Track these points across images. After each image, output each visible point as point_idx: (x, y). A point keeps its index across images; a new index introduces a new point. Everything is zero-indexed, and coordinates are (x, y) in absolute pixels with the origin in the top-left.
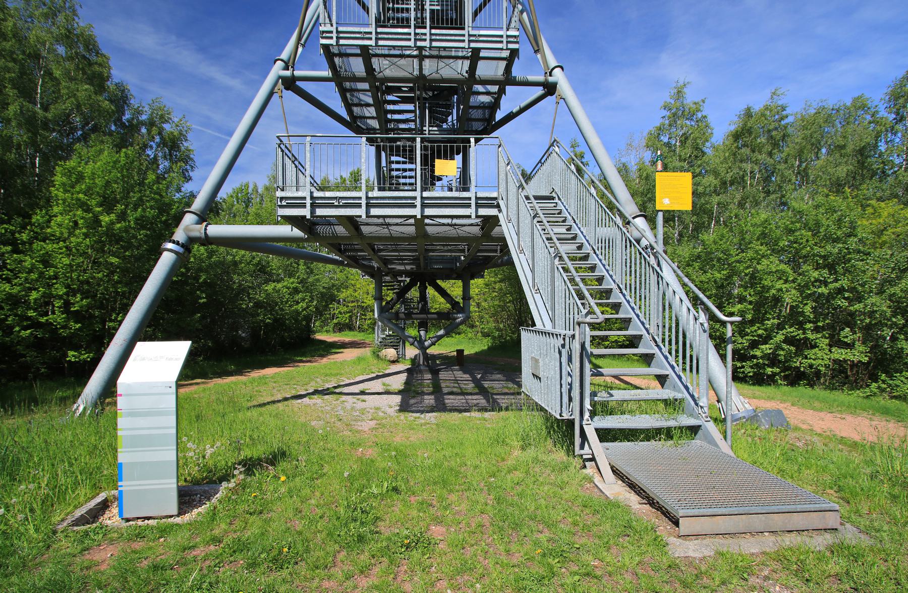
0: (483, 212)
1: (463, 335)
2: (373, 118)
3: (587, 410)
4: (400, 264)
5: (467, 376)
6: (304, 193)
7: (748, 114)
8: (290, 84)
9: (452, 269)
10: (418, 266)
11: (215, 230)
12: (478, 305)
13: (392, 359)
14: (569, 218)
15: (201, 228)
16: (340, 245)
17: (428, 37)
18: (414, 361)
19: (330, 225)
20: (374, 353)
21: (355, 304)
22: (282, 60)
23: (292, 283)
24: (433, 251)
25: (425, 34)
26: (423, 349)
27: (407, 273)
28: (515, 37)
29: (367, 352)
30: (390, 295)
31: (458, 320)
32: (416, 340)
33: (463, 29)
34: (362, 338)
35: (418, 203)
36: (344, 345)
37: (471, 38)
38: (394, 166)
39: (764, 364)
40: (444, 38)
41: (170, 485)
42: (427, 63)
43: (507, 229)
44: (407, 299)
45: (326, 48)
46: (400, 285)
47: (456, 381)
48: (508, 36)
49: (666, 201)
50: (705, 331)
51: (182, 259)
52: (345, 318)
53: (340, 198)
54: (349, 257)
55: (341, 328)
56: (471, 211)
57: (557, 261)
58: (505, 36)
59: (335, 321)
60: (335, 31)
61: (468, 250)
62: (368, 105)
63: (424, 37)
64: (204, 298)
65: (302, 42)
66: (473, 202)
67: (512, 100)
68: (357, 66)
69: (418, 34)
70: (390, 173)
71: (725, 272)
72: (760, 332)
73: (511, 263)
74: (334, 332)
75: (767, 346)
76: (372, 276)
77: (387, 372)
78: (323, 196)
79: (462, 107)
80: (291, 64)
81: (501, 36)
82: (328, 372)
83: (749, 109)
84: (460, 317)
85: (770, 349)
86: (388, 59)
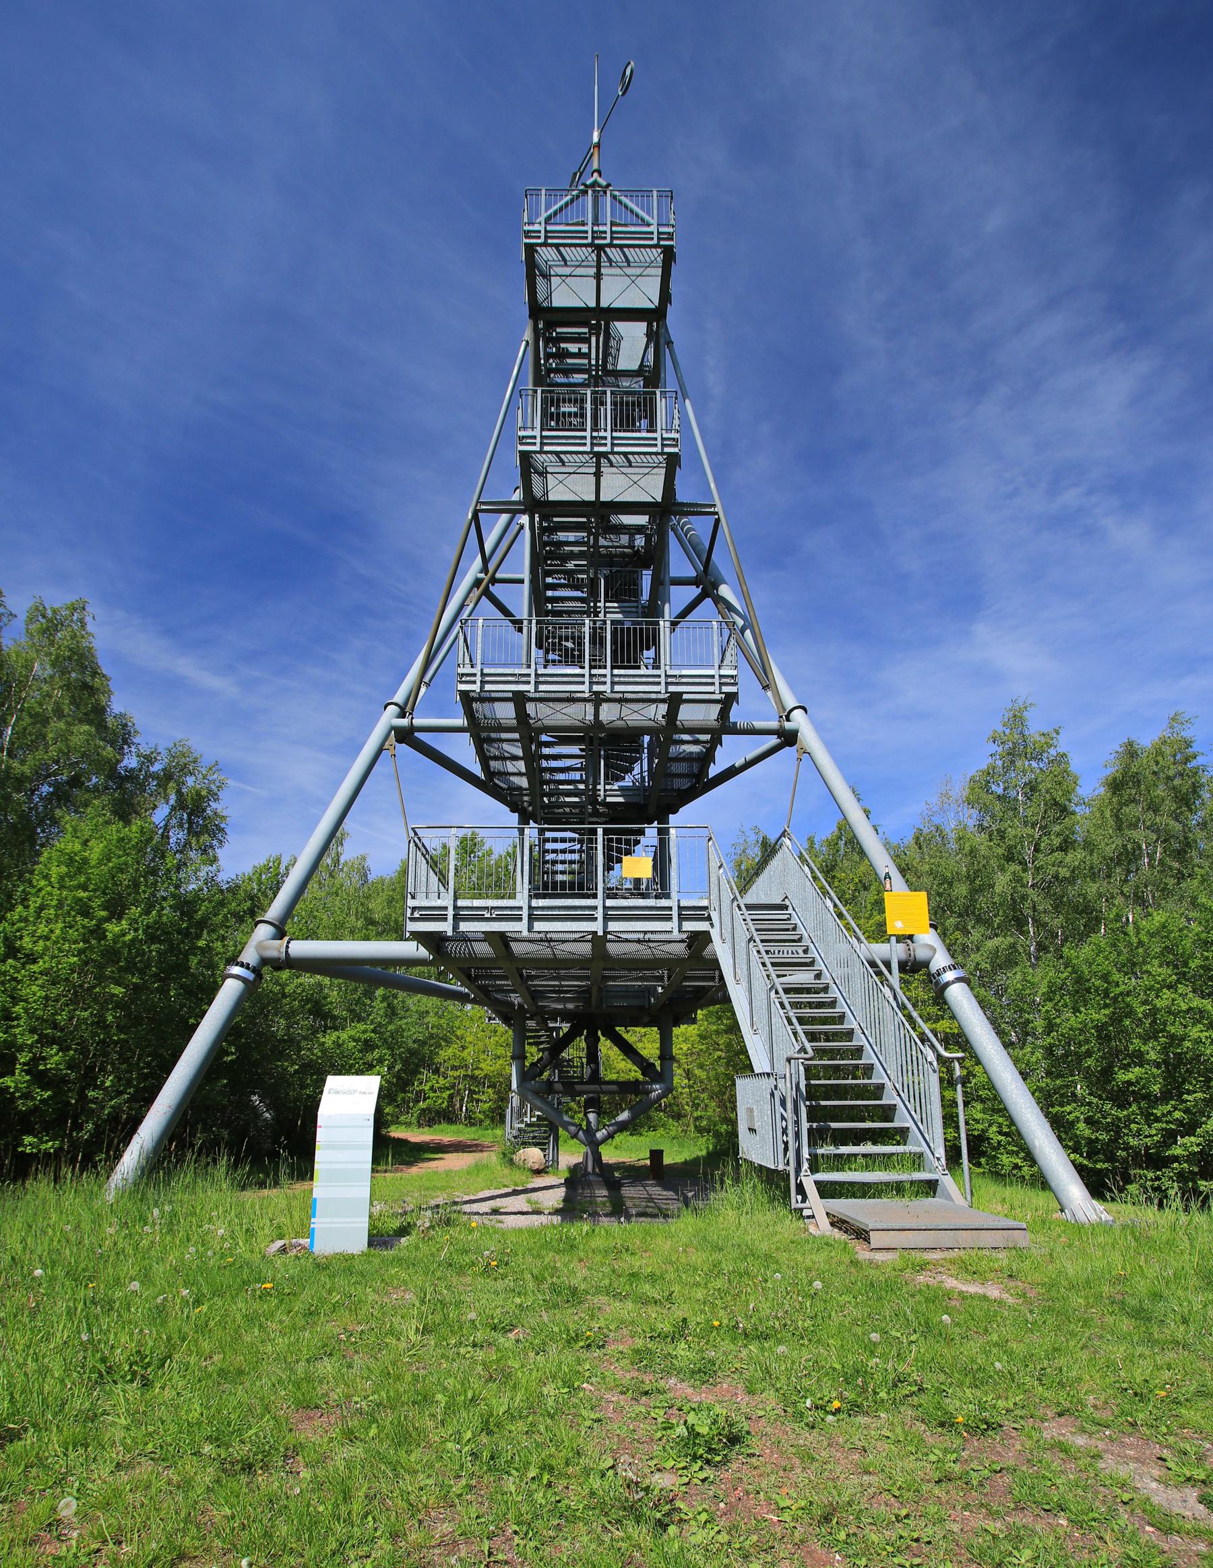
0: (689, 926)
1: (661, 1131)
2: (520, 774)
3: (805, 1160)
4: (559, 1000)
5: (670, 1194)
6: (447, 901)
7: (1131, 752)
8: (405, 736)
9: (641, 1008)
10: (588, 1001)
11: (301, 948)
12: (688, 1074)
13: (536, 1167)
14: (805, 935)
15: (281, 946)
16: (470, 968)
17: (608, 679)
18: (574, 1170)
19: (466, 941)
20: (504, 1154)
21: (462, 1072)
22: (396, 704)
23: (364, 1032)
24: (614, 978)
25: (605, 676)
26: (594, 1145)
27: (565, 1016)
28: (732, 677)
29: (492, 1158)
30: (533, 1054)
31: (653, 1095)
32: (581, 1128)
33: (668, 896)
34: (472, 1136)
35: (599, 914)
36: (441, 1148)
37: (670, 680)
38: (549, 846)
39: (1191, 1172)
40: (631, 680)
41: (362, 1225)
42: (605, 707)
43: (720, 949)
44: (564, 1060)
45: (465, 695)
46: (550, 1036)
47: (650, 1199)
48: (721, 676)
49: (899, 924)
50: (934, 1071)
51: (251, 989)
52: (440, 1100)
53: (493, 908)
54: (480, 988)
55: (431, 1118)
56: (673, 925)
57: (773, 994)
58: (717, 677)
59: (422, 1105)
60: (479, 674)
61: (669, 978)
62: (514, 758)
63: (603, 679)
64: (232, 1054)
65: (426, 679)
66: (675, 913)
67: (729, 752)
68: (506, 712)
69: (595, 675)
70: (544, 857)
71: (1107, 1012)
72: (1177, 1115)
73: (727, 1000)
74: (420, 1125)
75: (1193, 1139)
76: (506, 1020)
77: (530, 1186)
78: (470, 905)
79: (656, 761)
80: (408, 709)
81: (713, 677)
82: (428, 1183)
83: (1130, 744)
84: (657, 1089)
85: (1198, 1145)
86: (551, 704)
